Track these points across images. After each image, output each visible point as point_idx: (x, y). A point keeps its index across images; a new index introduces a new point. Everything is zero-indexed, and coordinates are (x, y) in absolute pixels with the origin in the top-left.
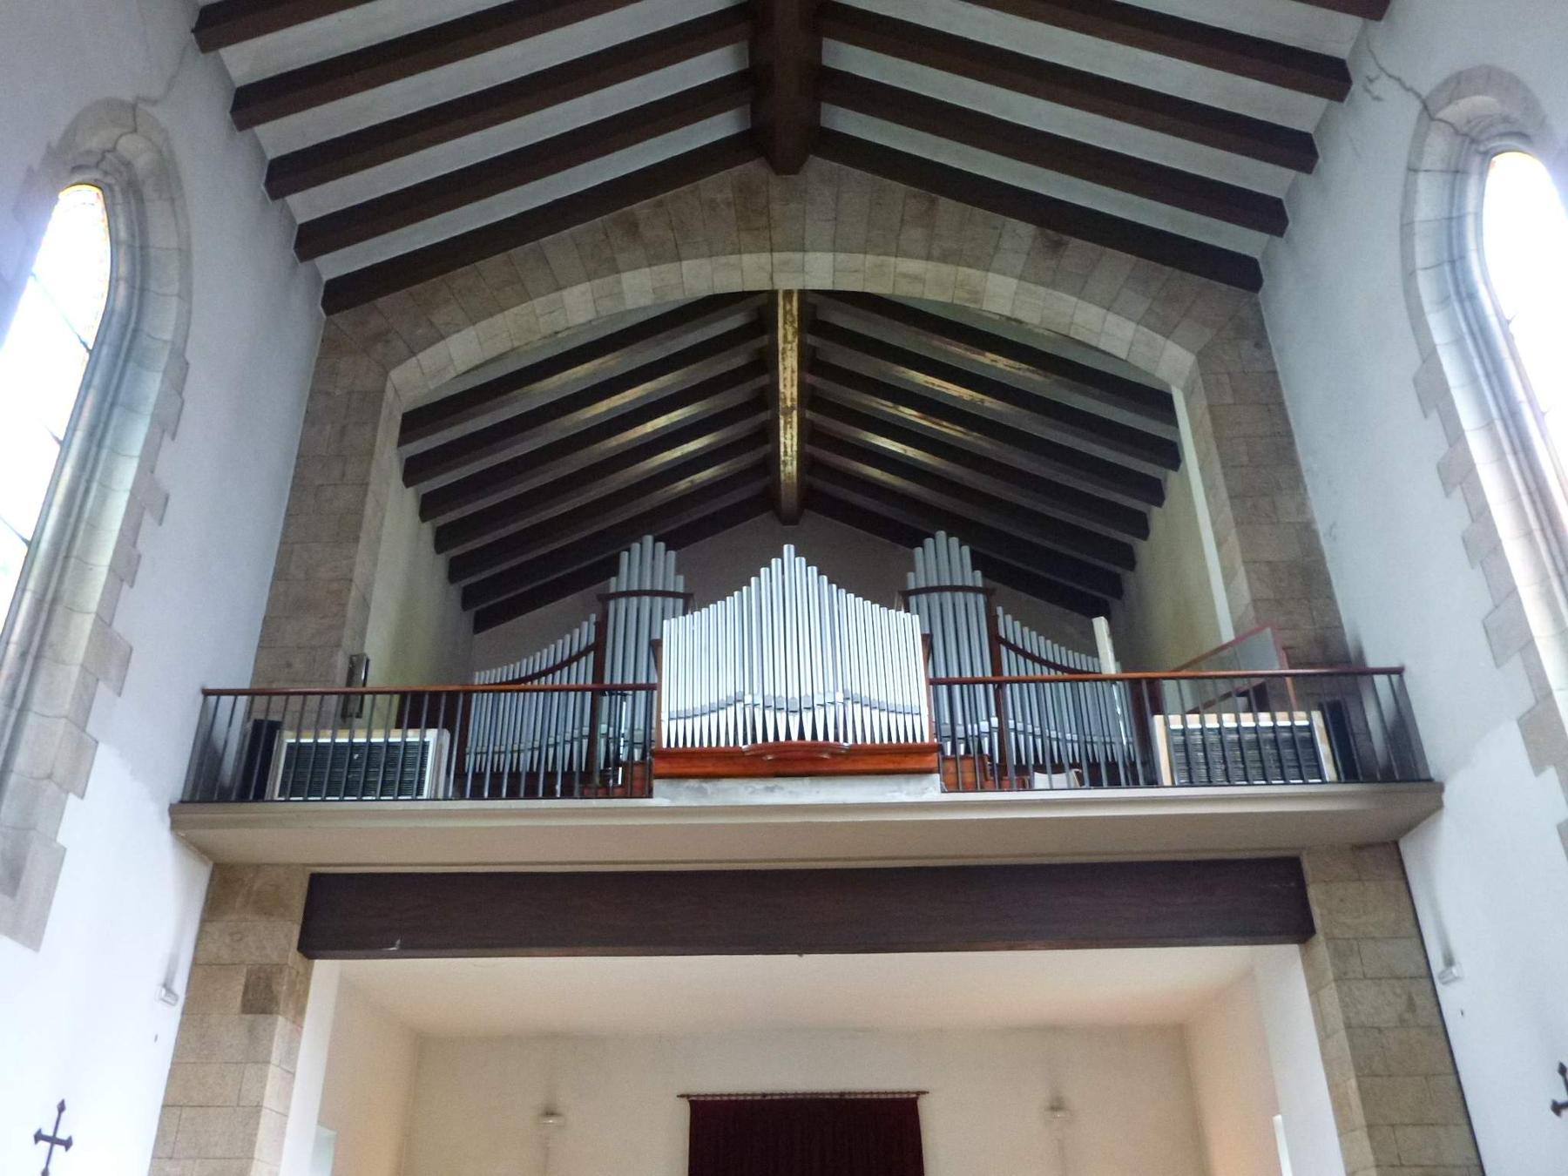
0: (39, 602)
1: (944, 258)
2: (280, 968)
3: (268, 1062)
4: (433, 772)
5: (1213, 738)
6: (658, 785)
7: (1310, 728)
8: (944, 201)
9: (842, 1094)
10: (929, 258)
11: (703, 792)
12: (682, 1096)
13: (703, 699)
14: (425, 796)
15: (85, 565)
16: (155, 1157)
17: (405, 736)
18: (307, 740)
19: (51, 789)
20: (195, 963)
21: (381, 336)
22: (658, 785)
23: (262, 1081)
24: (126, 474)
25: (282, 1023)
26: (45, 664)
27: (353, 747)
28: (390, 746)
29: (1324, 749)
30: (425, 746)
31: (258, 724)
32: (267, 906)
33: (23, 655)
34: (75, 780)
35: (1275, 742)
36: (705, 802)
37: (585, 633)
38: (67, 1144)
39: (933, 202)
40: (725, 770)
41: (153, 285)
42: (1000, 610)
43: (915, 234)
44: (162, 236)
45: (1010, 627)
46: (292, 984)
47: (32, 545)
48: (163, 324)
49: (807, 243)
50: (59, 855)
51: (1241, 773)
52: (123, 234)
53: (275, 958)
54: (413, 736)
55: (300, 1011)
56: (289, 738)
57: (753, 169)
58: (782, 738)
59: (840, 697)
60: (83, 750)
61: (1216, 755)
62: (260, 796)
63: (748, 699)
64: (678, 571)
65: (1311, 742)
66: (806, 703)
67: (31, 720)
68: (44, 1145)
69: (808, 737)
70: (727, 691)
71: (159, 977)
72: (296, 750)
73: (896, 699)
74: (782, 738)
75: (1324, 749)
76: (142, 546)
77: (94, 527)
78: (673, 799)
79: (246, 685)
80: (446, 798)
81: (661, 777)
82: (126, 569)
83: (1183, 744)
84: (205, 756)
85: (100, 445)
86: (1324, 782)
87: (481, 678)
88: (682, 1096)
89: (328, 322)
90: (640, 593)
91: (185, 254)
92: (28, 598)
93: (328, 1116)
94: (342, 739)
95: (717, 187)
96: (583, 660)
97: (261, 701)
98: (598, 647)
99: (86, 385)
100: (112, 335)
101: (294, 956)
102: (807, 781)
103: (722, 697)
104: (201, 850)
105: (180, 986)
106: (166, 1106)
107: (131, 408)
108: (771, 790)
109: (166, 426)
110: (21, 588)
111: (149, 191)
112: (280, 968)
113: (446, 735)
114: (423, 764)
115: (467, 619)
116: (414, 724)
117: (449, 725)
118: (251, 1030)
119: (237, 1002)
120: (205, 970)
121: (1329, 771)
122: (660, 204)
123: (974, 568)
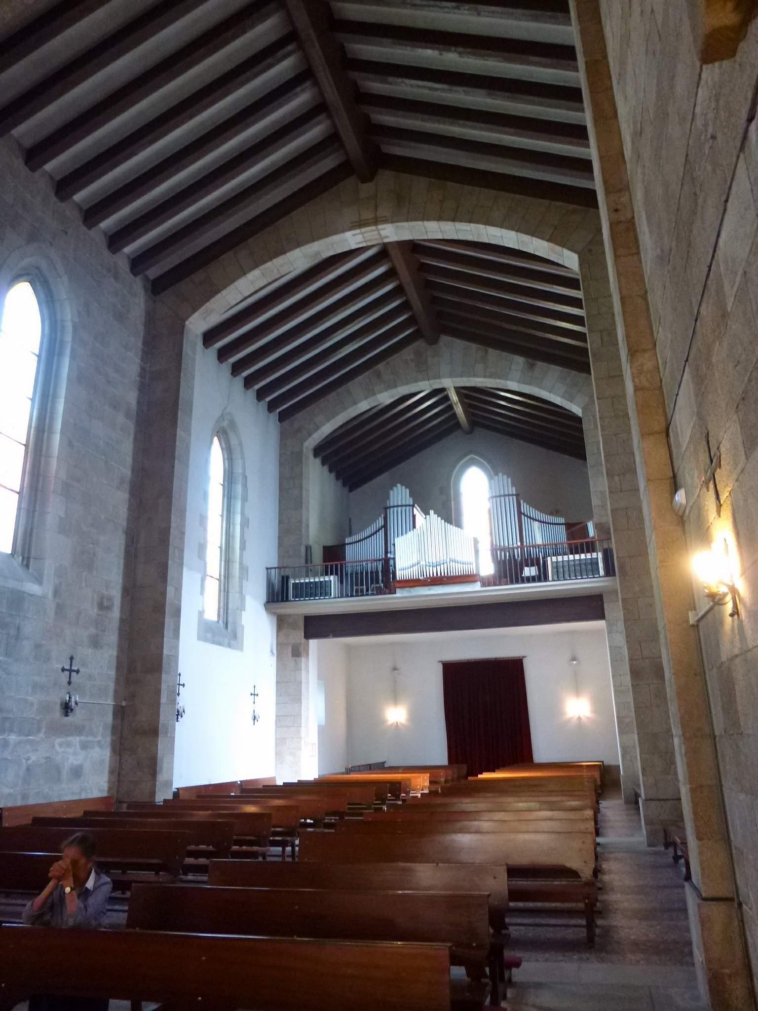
0: (225, 561)
1: (490, 377)
2: (300, 644)
3: (301, 670)
4: (334, 588)
5: (566, 564)
6: (398, 590)
7: (597, 558)
8: (490, 350)
9: (496, 658)
10: (485, 377)
11: (410, 591)
12: (439, 662)
13: (410, 563)
14: (332, 596)
15: (233, 548)
16: (277, 695)
17: (324, 579)
18: (297, 581)
19: (238, 611)
20: (277, 644)
21: (299, 430)
22: (398, 590)
23: (301, 675)
24: (238, 519)
25: (303, 659)
26: (230, 579)
27: (310, 583)
28: (321, 582)
29: (601, 565)
30: (330, 581)
31: (283, 577)
32: (293, 626)
33: (225, 577)
34: (242, 608)
35: (580, 565)
36: (412, 595)
37: (380, 522)
38: (257, 695)
39: (486, 352)
40: (416, 584)
41: (234, 457)
42: (522, 502)
43: (480, 367)
44: (234, 442)
45: (525, 507)
46: (304, 648)
47: (221, 548)
48: (238, 470)
49: (441, 374)
50: (243, 627)
51: (574, 575)
52: (224, 446)
53: (299, 641)
54: (327, 579)
55: (308, 655)
56: (292, 581)
57: (419, 344)
58: (431, 576)
59: (448, 561)
60: (242, 598)
61: (566, 569)
62: (287, 600)
63: (421, 563)
64: (410, 496)
65: (597, 563)
66: (438, 563)
67: (230, 595)
68: (253, 696)
69: (439, 575)
70: (415, 561)
71: (269, 650)
72: (295, 585)
73: (465, 560)
74: (431, 576)
75: (601, 565)
76: (245, 537)
77: (233, 536)
78: (402, 594)
79: (276, 565)
80: (338, 597)
81: (398, 588)
82: (243, 548)
83: (556, 566)
84: (270, 585)
85: (230, 512)
86: (600, 577)
87: (347, 540)
88: (439, 662)
89: (281, 426)
90: (398, 506)
91: (241, 444)
92: (223, 562)
93: (320, 677)
94: (307, 581)
95: (407, 353)
96: (381, 531)
97: (282, 570)
98: (385, 526)
99: (224, 496)
100: (226, 479)
101: (303, 640)
102: (440, 586)
103: (414, 563)
104: (274, 613)
105: (275, 651)
106: (277, 682)
107: (235, 498)
108: (430, 590)
109: (245, 499)
110: (221, 560)
111: (229, 431)
112: (300, 644)
113: (337, 577)
114: (331, 587)
115: (346, 489)
116: (327, 574)
117: (337, 574)
118: (295, 661)
119: (290, 654)
120: (281, 646)
121: (602, 572)
122: (388, 363)
123: (512, 486)
